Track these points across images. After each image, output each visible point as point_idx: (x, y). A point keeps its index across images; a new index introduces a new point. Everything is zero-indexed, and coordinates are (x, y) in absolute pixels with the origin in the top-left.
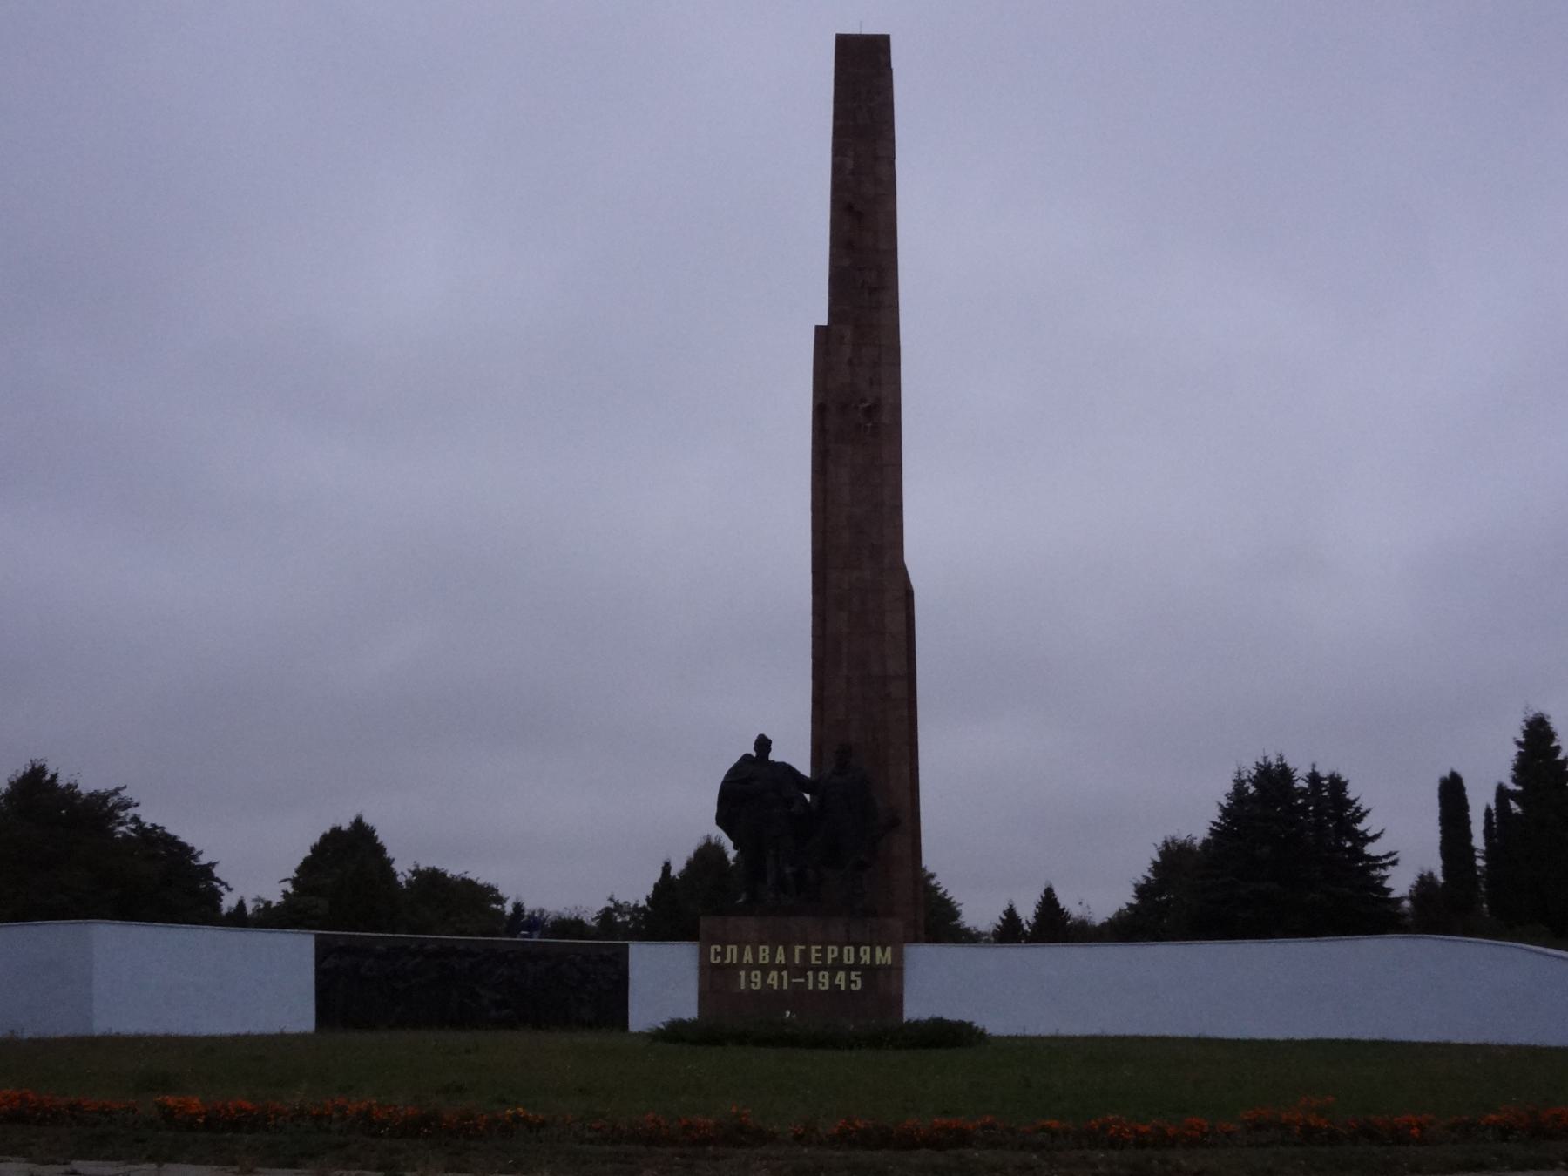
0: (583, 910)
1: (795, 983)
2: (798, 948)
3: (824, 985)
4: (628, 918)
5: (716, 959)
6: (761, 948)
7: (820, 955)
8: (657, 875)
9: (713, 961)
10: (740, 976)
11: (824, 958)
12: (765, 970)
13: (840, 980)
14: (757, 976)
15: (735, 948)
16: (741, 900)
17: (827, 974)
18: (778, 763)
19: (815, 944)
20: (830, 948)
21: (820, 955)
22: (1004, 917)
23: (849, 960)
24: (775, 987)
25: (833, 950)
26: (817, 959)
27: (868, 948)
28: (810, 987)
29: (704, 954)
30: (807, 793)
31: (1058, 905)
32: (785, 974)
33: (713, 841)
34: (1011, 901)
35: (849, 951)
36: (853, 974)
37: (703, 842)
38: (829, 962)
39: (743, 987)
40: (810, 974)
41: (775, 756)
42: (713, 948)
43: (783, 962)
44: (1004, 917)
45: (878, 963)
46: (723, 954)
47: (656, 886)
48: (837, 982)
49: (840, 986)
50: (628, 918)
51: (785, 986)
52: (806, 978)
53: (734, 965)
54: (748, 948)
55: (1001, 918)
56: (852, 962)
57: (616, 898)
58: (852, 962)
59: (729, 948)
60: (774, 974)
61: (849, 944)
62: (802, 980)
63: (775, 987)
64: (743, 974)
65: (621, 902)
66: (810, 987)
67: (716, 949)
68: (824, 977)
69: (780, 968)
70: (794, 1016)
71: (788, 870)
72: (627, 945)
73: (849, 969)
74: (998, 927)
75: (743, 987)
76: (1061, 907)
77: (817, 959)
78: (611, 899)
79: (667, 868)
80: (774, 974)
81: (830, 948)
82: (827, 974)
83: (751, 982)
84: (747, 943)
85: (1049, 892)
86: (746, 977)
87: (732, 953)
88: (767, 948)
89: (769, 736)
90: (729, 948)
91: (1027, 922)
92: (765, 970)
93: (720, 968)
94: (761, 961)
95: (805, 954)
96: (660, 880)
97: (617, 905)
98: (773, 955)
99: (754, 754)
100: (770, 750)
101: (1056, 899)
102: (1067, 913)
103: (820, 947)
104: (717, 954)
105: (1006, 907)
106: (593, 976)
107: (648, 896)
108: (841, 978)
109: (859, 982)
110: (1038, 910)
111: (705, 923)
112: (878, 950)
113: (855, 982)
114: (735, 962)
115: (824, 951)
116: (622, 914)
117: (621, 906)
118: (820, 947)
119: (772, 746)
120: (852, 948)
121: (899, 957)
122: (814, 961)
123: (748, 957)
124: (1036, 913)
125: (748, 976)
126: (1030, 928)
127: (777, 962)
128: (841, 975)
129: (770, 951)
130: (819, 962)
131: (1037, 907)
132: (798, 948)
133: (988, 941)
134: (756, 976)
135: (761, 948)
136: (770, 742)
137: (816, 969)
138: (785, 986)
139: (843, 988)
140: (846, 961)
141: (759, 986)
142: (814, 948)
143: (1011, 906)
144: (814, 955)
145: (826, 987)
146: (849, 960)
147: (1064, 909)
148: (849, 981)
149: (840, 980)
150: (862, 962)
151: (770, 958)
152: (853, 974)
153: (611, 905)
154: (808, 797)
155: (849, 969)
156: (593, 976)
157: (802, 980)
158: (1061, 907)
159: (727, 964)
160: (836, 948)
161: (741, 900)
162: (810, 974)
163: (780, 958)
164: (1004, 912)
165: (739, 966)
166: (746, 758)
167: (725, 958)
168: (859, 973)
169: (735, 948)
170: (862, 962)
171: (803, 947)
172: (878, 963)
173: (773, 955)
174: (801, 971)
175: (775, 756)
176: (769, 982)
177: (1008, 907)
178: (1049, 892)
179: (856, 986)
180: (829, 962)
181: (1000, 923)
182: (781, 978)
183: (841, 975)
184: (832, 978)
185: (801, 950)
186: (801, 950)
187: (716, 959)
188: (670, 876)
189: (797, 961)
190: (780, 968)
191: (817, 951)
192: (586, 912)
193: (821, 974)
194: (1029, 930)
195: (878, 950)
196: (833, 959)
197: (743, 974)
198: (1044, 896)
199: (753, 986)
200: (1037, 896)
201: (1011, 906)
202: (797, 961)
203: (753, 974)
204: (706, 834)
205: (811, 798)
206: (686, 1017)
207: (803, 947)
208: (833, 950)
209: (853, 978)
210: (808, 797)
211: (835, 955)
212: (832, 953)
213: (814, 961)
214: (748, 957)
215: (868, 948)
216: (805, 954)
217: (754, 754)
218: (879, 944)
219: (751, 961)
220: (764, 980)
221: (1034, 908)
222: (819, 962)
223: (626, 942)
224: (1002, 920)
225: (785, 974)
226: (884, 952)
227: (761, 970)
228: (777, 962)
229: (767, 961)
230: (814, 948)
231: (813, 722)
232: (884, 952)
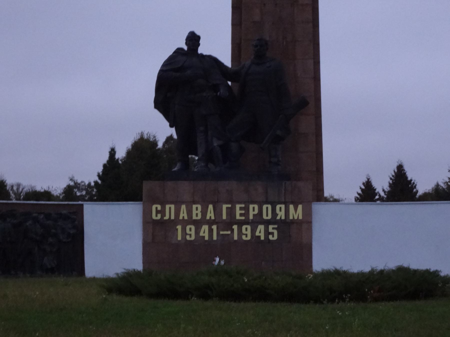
0: (53, 189)
1: (222, 235)
2: (225, 207)
3: (246, 235)
4: (84, 193)
5: (156, 216)
6: (194, 206)
7: (243, 212)
8: (105, 158)
9: (154, 217)
10: (177, 230)
11: (246, 214)
12: (198, 224)
13: (260, 232)
14: (191, 230)
15: (173, 206)
16: (176, 169)
17: (249, 227)
18: (206, 56)
19: (240, 203)
20: (251, 206)
21: (243, 212)
22: (363, 187)
23: (267, 215)
24: (207, 238)
25: (254, 208)
26: (241, 215)
27: (283, 206)
28: (236, 238)
29: (147, 214)
30: (230, 81)
31: (407, 178)
32: (214, 227)
33: (145, 137)
34: (368, 175)
35: (267, 209)
36: (271, 227)
37: (138, 137)
38: (251, 217)
39: (179, 238)
40: (235, 227)
41: (202, 50)
42: (154, 207)
43: (213, 218)
44: (363, 187)
45: (291, 218)
46: (163, 212)
47: (105, 166)
48: (257, 234)
49: (204, 237)
50: (84, 193)
51: (215, 238)
52: (232, 231)
53: (173, 220)
54: (183, 207)
55: (361, 188)
56: (270, 217)
57: (75, 178)
58: (270, 217)
59: (167, 207)
60: (205, 228)
61: (267, 202)
62: (229, 232)
63: (207, 238)
64: (179, 227)
65: (79, 181)
66: (236, 238)
67: (157, 208)
68: (247, 230)
69: (210, 223)
70: (222, 263)
71: (216, 143)
72: (82, 205)
73: (267, 223)
74: (359, 194)
75: (179, 238)
76: (409, 179)
77: (241, 215)
78: (71, 180)
79: (112, 152)
80: (205, 228)
81: (251, 206)
82: (249, 227)
83: (186, 234)
84: (183, 203)
85: (400, 168)
86: (182, 229)
87: (170, 208)
88: (199, 207)
89: (198, 33)
90: (167, 207)
91: (383, 190)
92: (198, 224)
93: (161, 223)
94: (194, 217)
95: (231, 211)
96: (108, 161)
97: (76, 183)
98: (204, 213)
99: (186, 48)
100: (199, 45)
101: (405, 173)
102: (414, 183)
103: (243, 206)
104: (157, 212)
105: (365, 180)
106: (53, 231)
107: (99, 174)
108: (260, 231)
109: (276, 232)
110: (391, 182)
111: (147, 186)
112: (291, 207)
113: (272, 234)
114: (173, 217)
115: (247, 209)
116: (80, 189)
117: (79, 184)
118: (243, 206)
119: (201, 42)
120: (270, 207)
121: (308, 213)
122: (238, 217)
123: (183, 215)
124: (390, 184)
125: (184, 229)
126: (385, 194)
127: (208, 218)
128: (261, 228)
129: (202, 208)
130: (243, 218)
131: (391, 179)
132: (225, 207)
133: (381, 199)
134: (190, 229)
135: (194, 206)
136: (199, 38)
137: (240, 224)
138: (215, 238)
139: (262, 238)
140: (265, 217)
141: (193, 238)
142: (238, 206)
143: (368, 179)
144: (238, 212)
145: (249, 238)
146: (267, 215)
147: (411, 180)
148: (267, 233)
149: (260, 232)
150: (278, 218)
151: (202, 215)
152: (271, 227)
153: (72, 184)
154: (230, 83)
155: (267, 223)
156: (53, 231)
157: (229, 232)
158: (409, 179)
159: (166, 220)
160: (256, 207)
161: (176, 169)
162: (235, 227)
163: (211, 214)
164: (363, 184)
165: (173, 223)
166: (179, 51)
167: (165, 216)
168: (276, 226)
169: (173, 206)
170: (278, 218)
171: (229, 206)
172: (291, 218)
173: (204, 213)
174: (228, 225)
175: (202, 50)
176: (201, 234)
177: (367, 180)
178: (400, 168)
179: (273, 236)
180: (251, 217)
181: (360, 192)
182: (211, 231)
183: (261, 228)
184: (253, 231)
185: (227, 208)
186: (227, 208)
187: (156, 216)
188: (115, 158)
189: (224, 217)
190: (210, 223)
191: (241, 209)
192: (56, 190)
193: (244, 227)
194: (385, 196)
195: (291, 207)
196: (254, 215)
197: (179, 227)
198: (396, 171)
199: (271, 237)
200: (391, 171)
201: (368, 179)
202: (224, 217)
203: (188, 227)
204: (140, 132)
205: (231, 84)
206: (139, 270)
207: (229, 206)
208: (254, 208)
209: (271, 230)
210: (230, 83)
211: (256, 212)
212: (253, 209)
213: (238, 217)
214: (183, 215)
215: (283, 206)
216: (231, 211)
217: (186, 48)
218: (292, 203)
219: (186, 218)
220: (197, 232)
221: (389, 180)
222: (243, 218)
223: (80, 202)
224: (362, 190)
225: (214, 227)
226: (296, 209)
227: (194, 225)
228: (208, 218)
229: (199, 217)
230: (238, 206)
231: (233, 25)
232: (296, 209)
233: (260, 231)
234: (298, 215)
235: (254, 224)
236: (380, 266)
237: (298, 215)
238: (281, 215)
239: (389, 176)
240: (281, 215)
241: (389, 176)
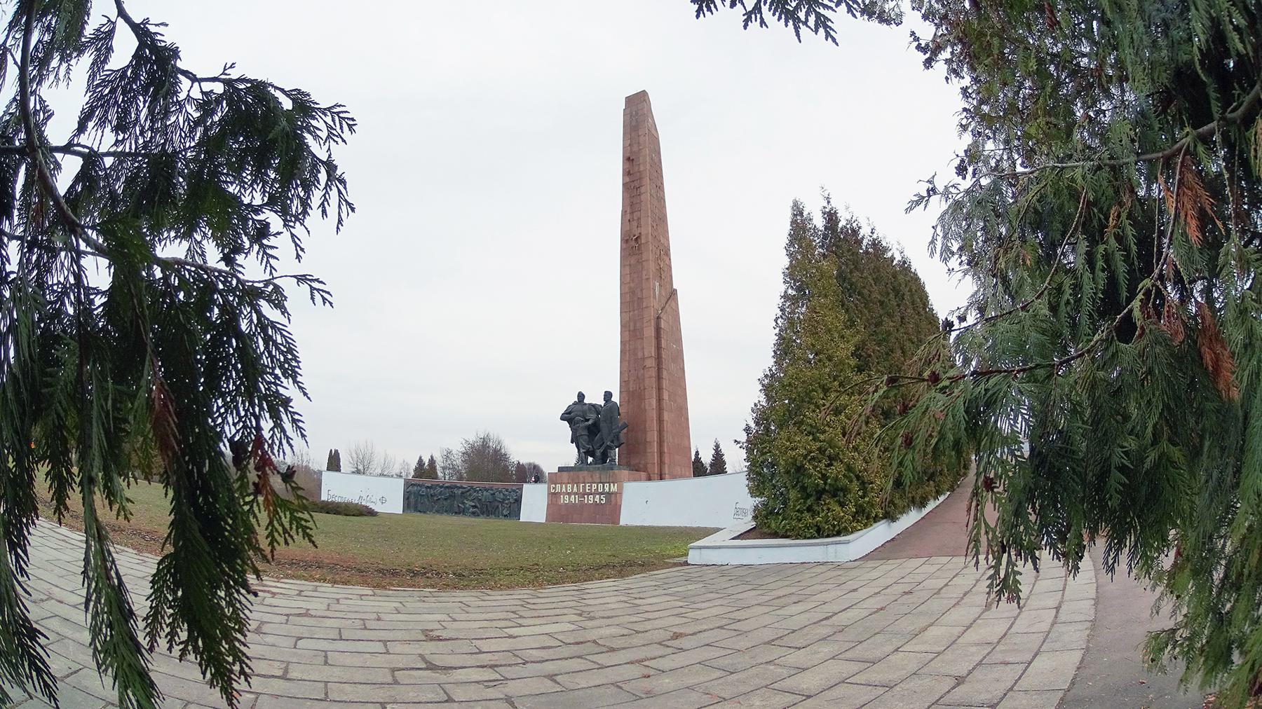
11: (591, 489)
29: (549, 488)
60: (573, 496)
69: (575, 494)
73: (601, 494)
144: (587, 488)
155: (601, 494)
163: (575, 490)
165: (560, 494)
174: (583, 495)
175: (586, 401)
190: (575, 494)
233: (597, 500)
234: (733, 539)
235: (597, 493)
236: (629, 524)
237: (733, 539)
238: (607, 489)
239: (798, 211)
240: (607, 489)
241: (798, 211)
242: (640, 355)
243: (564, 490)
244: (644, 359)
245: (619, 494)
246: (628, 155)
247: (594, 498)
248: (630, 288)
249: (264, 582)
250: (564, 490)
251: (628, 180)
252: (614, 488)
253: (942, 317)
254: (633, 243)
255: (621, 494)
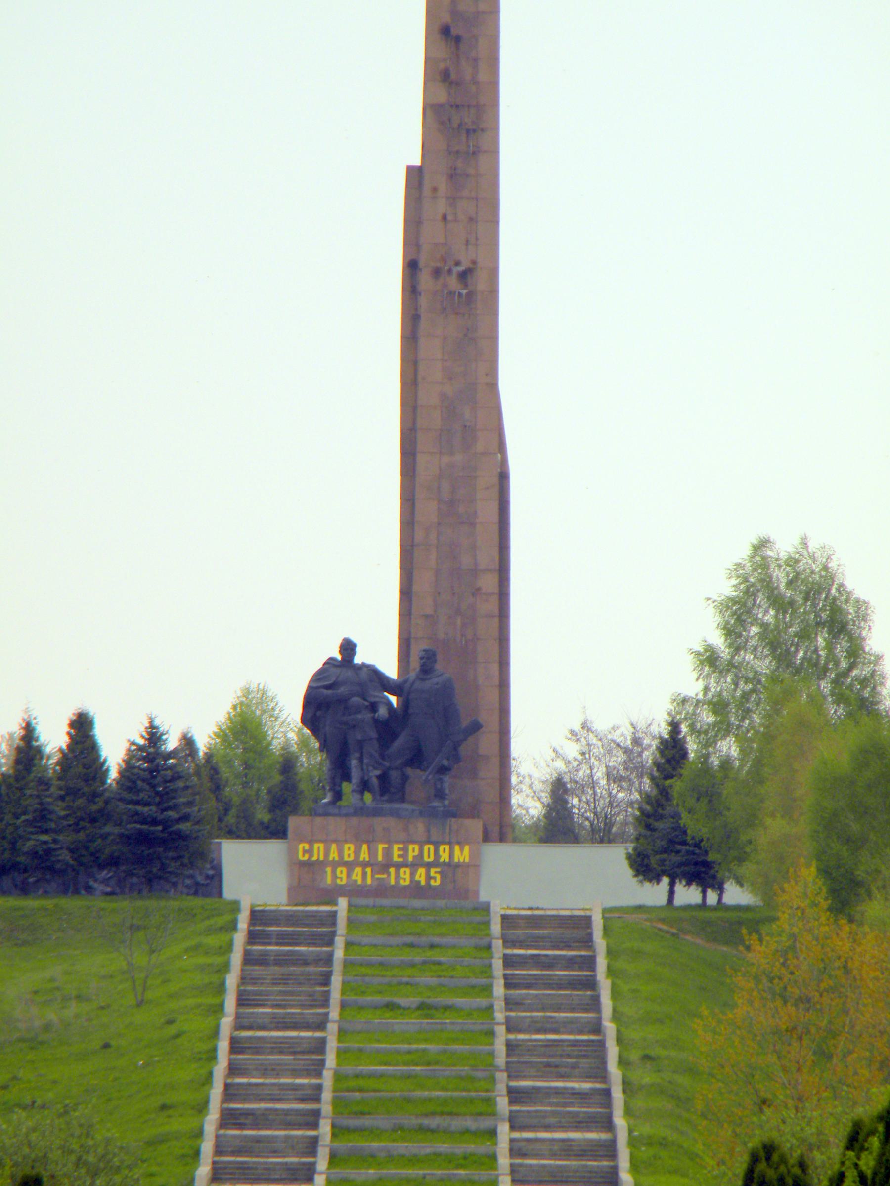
11: (405, 856)
29: (292, 852)
60: (358, 870)
69: (364, 865)
73: (429, 866)
163: (364, 855)
174: (385, 867)
175: (358, 660)
190: (364, 865)
235: (414, 866)
238: (444, 857)
240: (444, 857)
241: (29, 733)
242: (466, 561)
243: (334, 855)
244: (475, 572)
245: (474, 866)
246: (446, 18)
247: (413, 874)
248: (443, 396)
249: (37, 800)
250: (334, 855)
251: (442, 96)
252: (462, 855)
253: (228, 893)
254: (453, 282)
255: (478, 866)
